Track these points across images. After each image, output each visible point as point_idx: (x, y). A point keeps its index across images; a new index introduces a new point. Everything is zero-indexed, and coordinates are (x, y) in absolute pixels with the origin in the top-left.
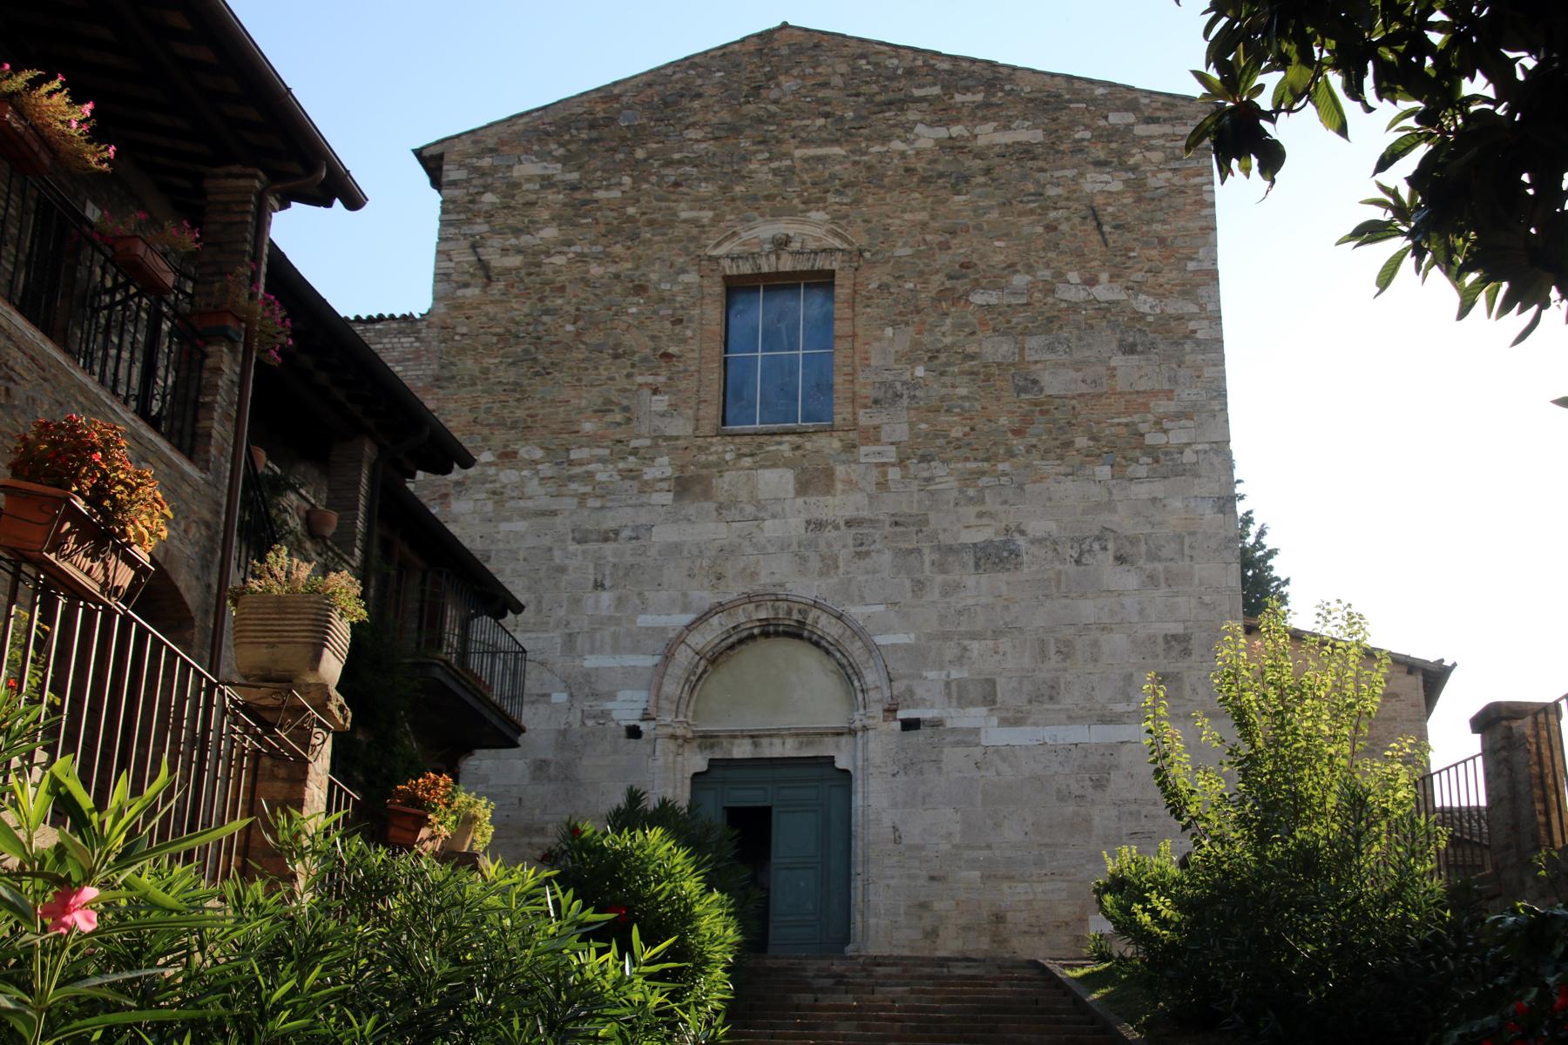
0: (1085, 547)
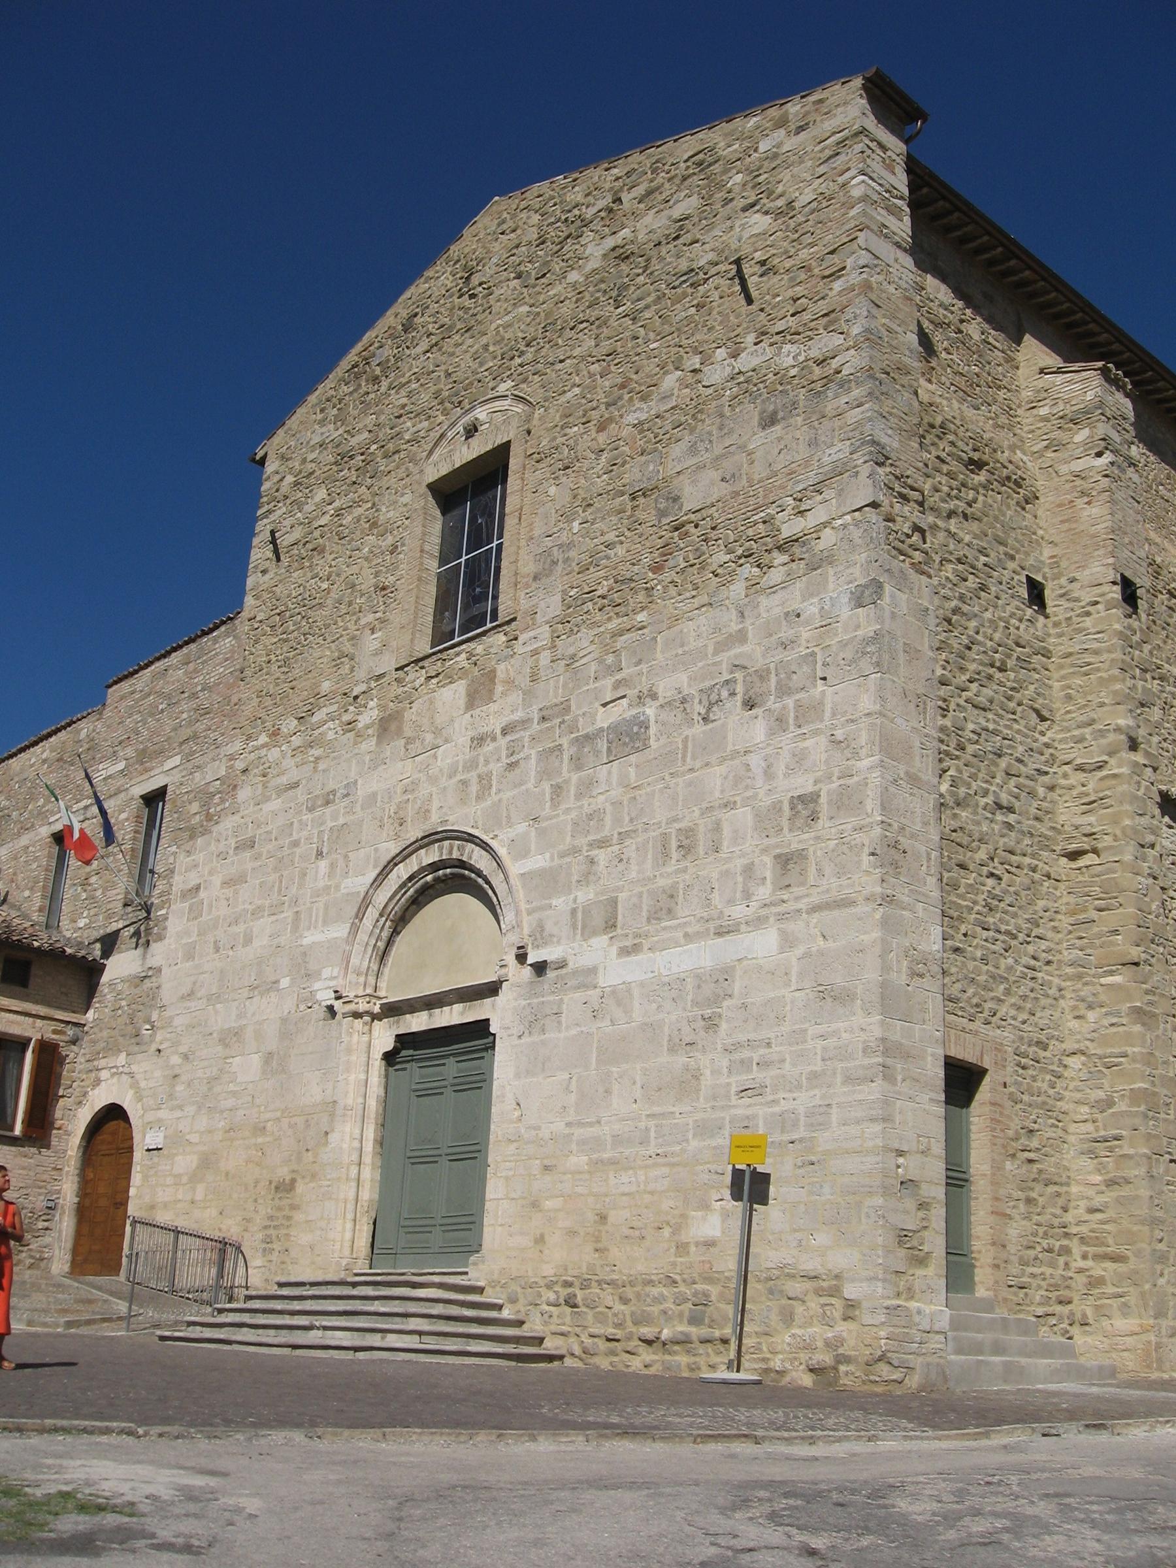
0: (714, 697)
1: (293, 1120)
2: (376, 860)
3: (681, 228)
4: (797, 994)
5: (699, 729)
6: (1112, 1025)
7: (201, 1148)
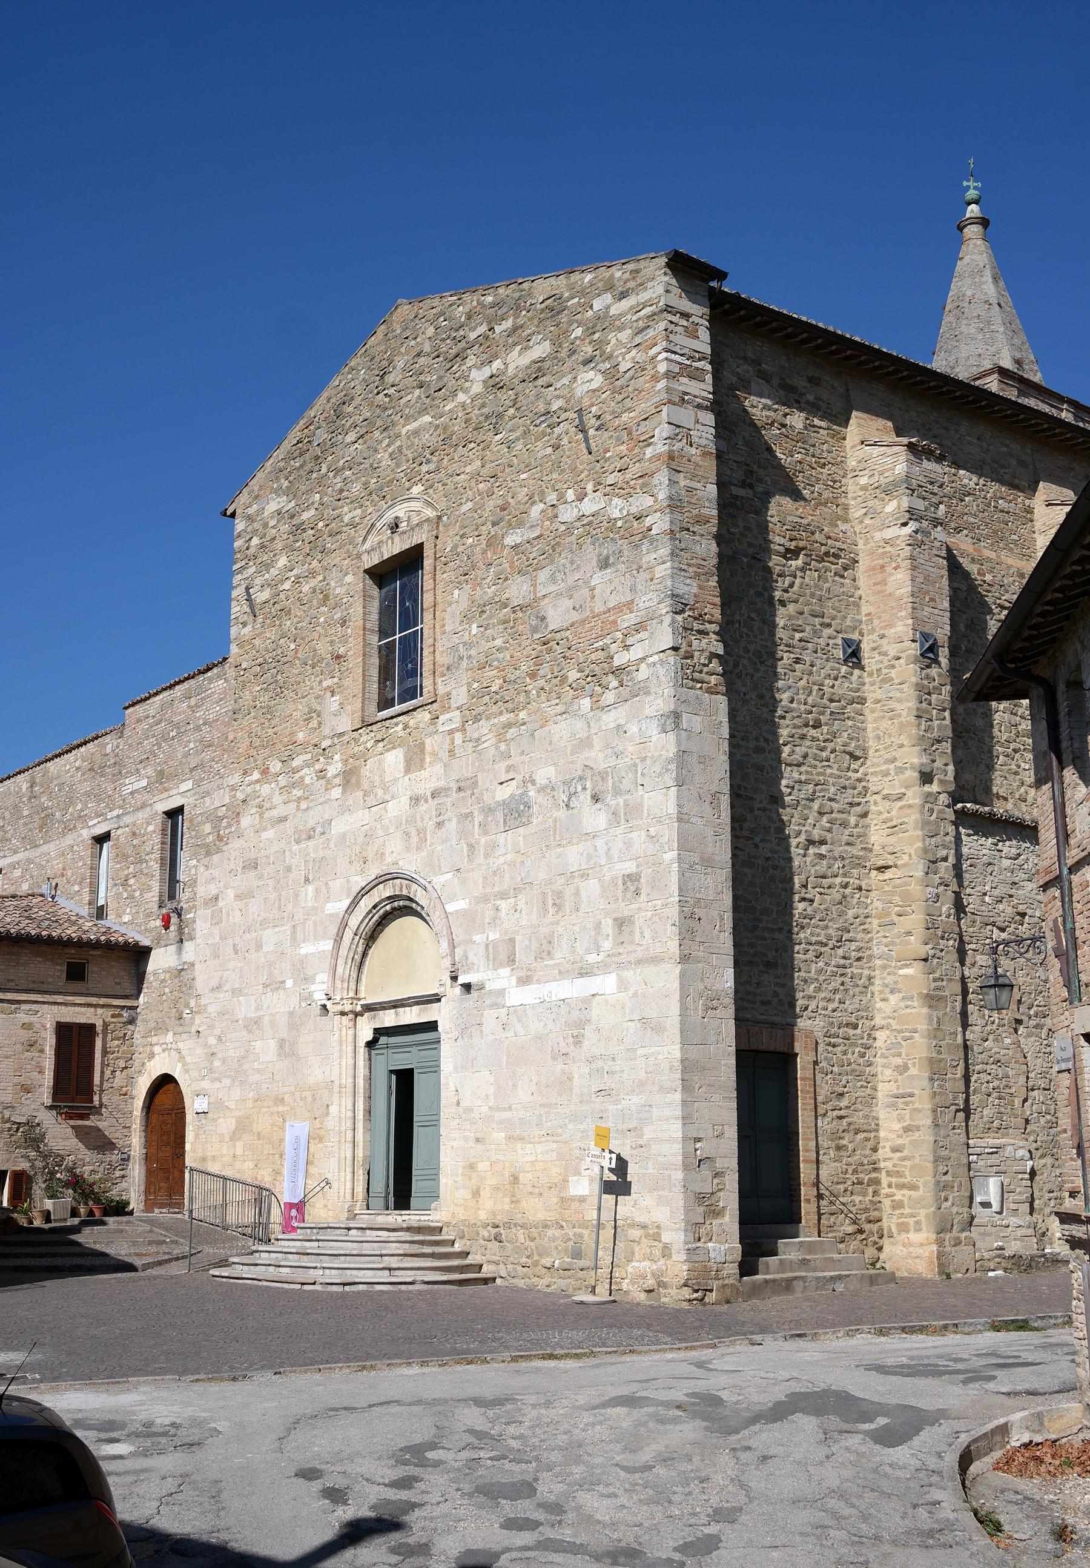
0: (572, 790)
1: (304, 1094)
2: (349, 889)
3: (539, 369)
4: (630, 1023)
5: (562, 813)
6: (907, 1007)
7: (238, 1113)
